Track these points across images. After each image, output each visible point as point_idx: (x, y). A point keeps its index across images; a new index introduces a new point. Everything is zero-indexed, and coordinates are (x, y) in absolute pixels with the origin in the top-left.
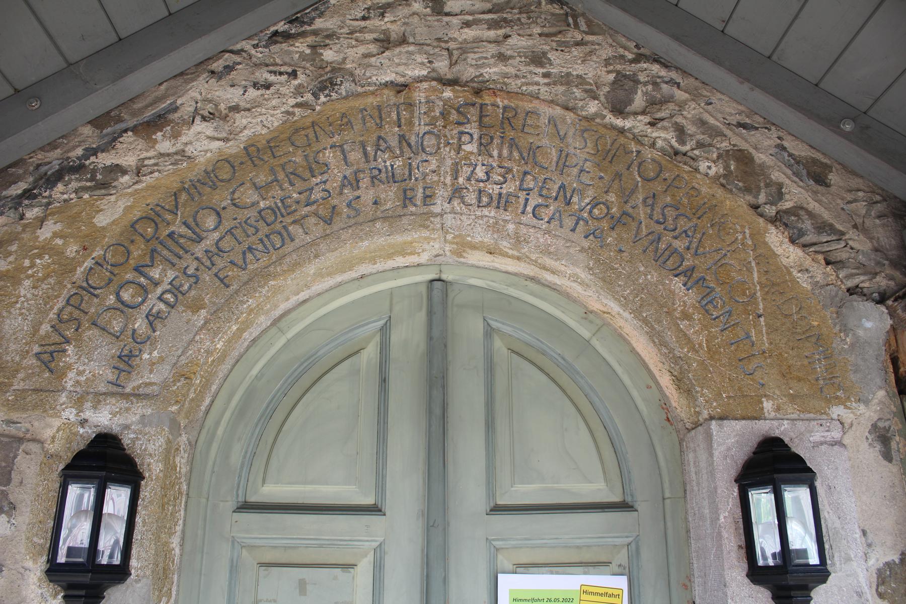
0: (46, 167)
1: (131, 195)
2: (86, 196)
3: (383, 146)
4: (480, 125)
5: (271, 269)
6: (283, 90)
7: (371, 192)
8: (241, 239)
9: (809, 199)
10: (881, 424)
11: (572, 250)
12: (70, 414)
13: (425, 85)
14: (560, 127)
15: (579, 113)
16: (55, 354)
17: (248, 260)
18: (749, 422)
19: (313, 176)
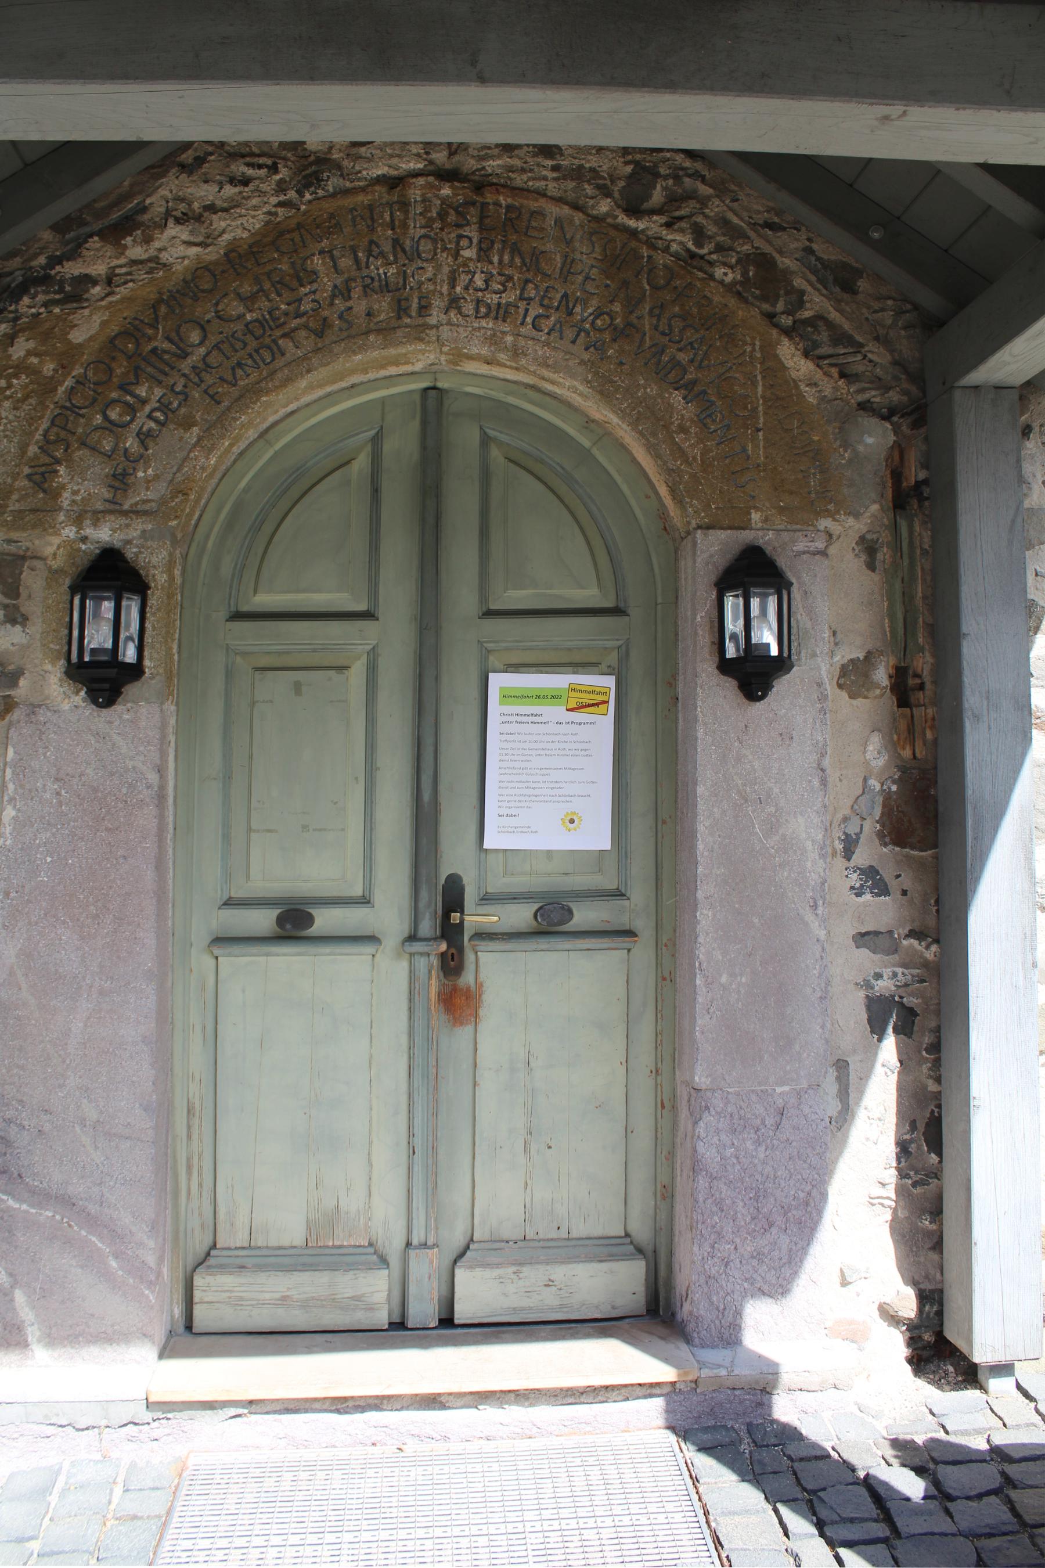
0: (8, 279)
1: (107, 308)
2: (57, 310)
3: (376, 251)
4: (480, 227)
5: (263, 384)
6: (264, 187)
7: (364, 303)
8: (229, 354)
9: (831, 308)
10: (869, 537)
11: (571, 363)
12: (70, 532)
13: (421, 181)
14: (566, 229)
15: (590, 212)
16: (46, 475)
17: (238, 376)
18: (734, 532)
19: (302, 285)
